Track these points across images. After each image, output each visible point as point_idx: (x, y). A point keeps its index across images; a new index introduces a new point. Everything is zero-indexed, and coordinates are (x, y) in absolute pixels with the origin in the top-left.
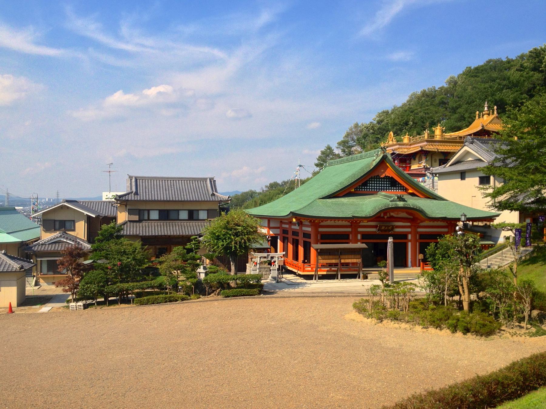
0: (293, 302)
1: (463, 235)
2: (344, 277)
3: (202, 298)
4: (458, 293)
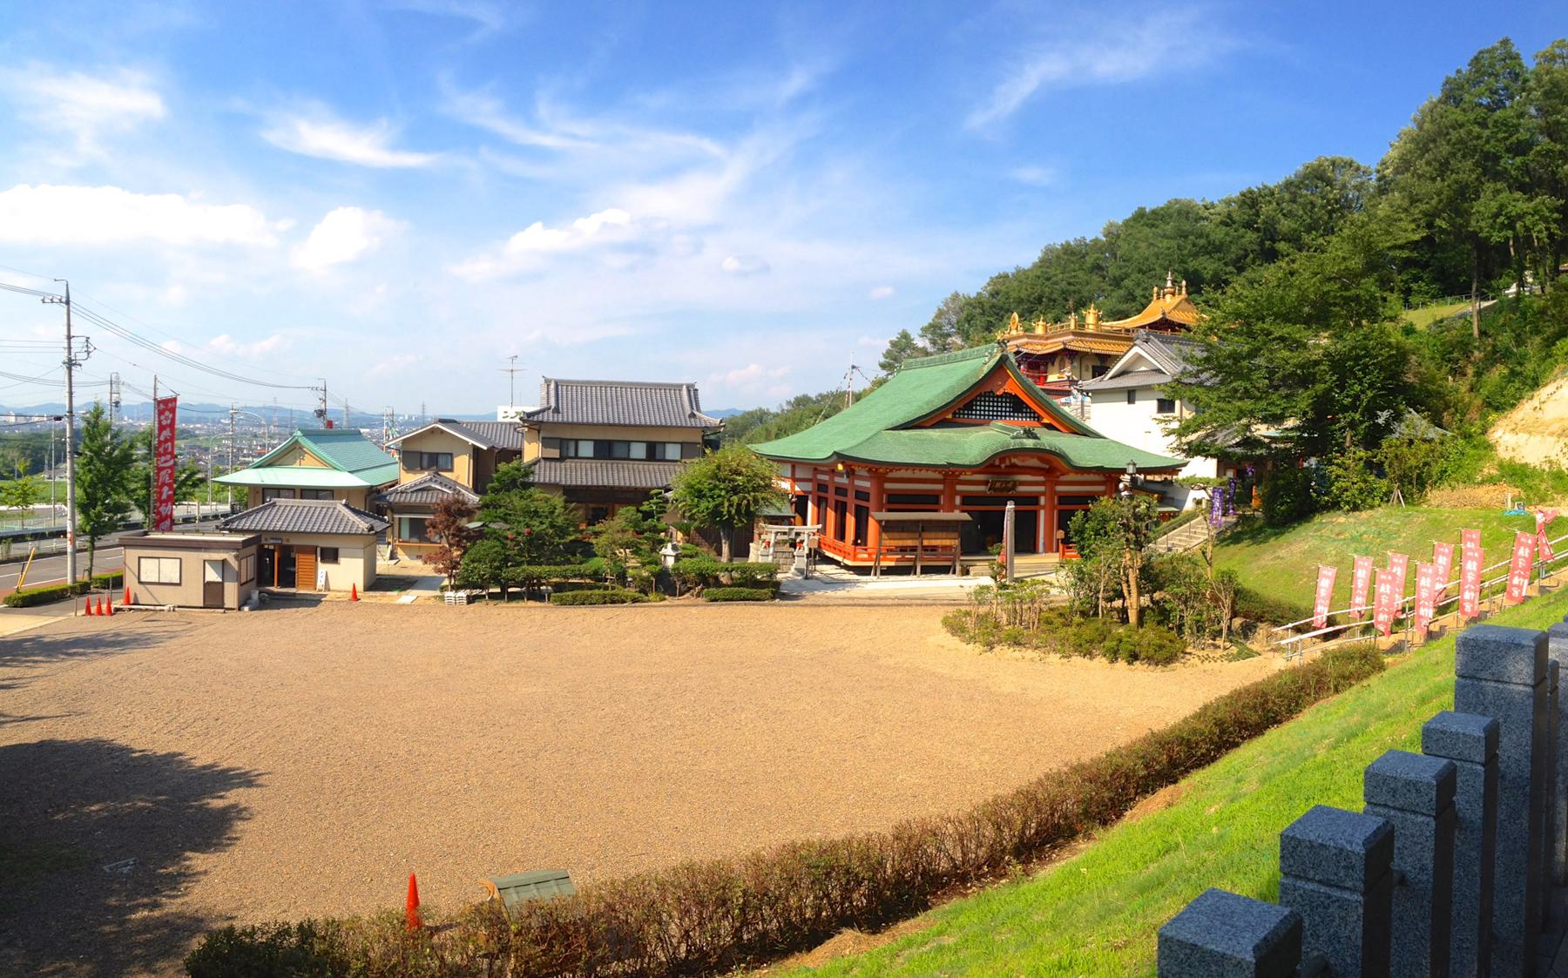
0: (835, 613)
1: (1131, 498)
2: (926, 570)
3: (669, 600)
4: (1120, 595)
